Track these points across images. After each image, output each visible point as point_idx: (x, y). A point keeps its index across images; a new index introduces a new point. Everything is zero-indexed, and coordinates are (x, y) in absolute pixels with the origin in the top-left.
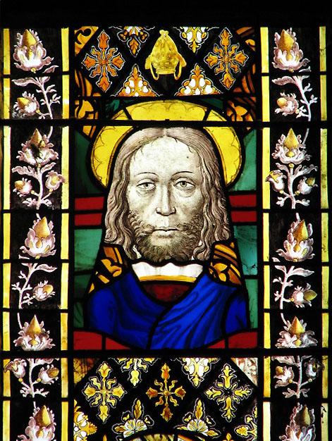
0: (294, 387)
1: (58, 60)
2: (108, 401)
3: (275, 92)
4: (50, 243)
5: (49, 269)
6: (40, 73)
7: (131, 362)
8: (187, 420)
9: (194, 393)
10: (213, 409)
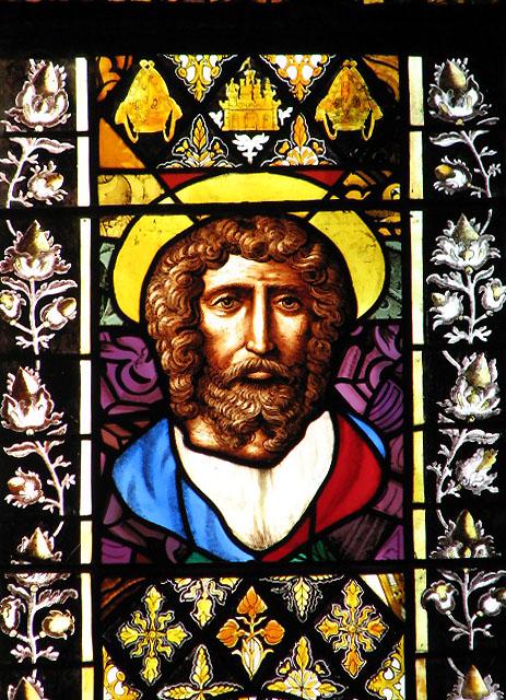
0: (464, 326)
1: (72, 418)
2: (160, 649)
3: (432, 156)
4: (62, 102)
5: (56, 147)
6: (41, 435)
7: (198, 586)
8: (284, 671)
9: (297, 627)
10: (325, 653)
